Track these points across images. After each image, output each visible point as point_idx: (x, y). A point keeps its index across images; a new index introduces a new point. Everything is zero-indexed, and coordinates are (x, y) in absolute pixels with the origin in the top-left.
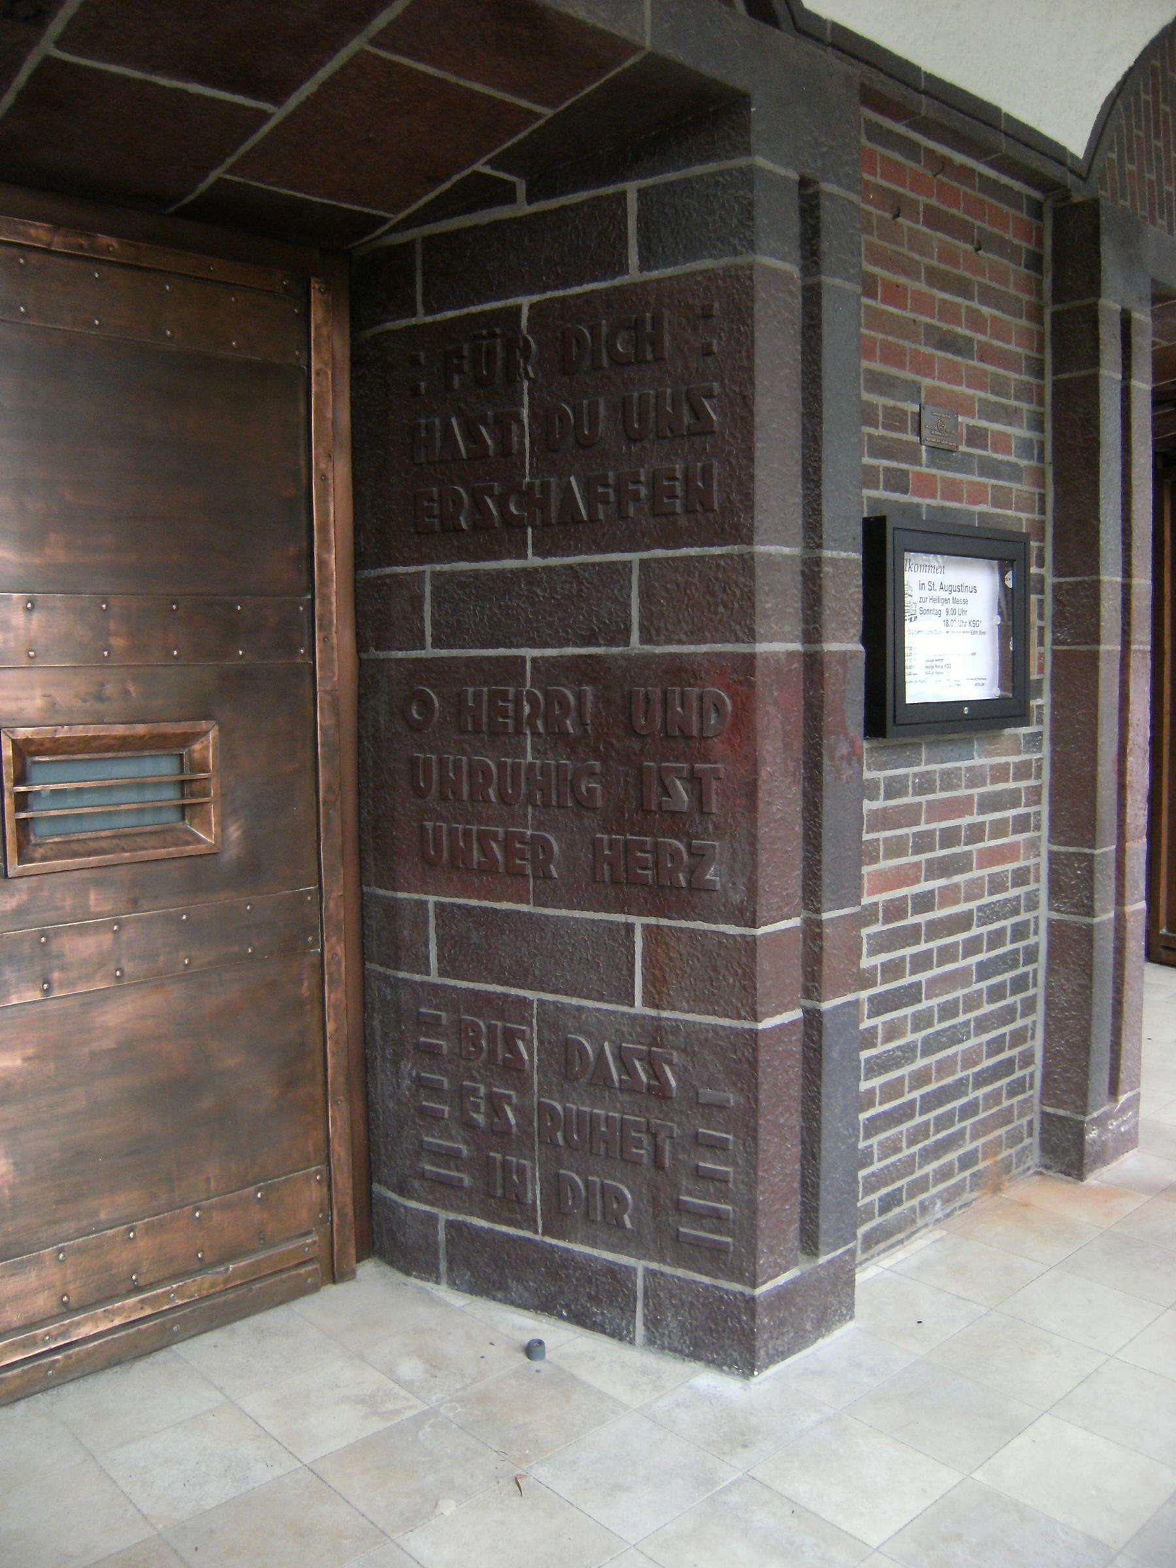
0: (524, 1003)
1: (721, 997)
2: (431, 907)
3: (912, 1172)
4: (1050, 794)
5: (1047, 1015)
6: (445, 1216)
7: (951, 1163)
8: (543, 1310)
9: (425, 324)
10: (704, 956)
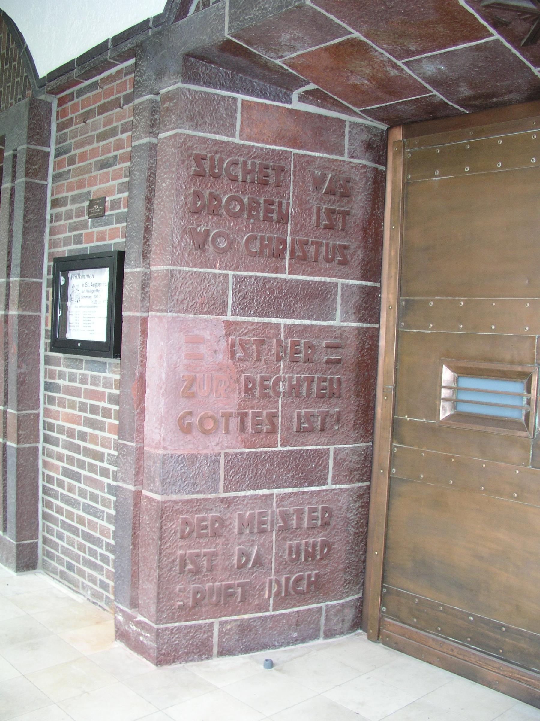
2: (237, 134)
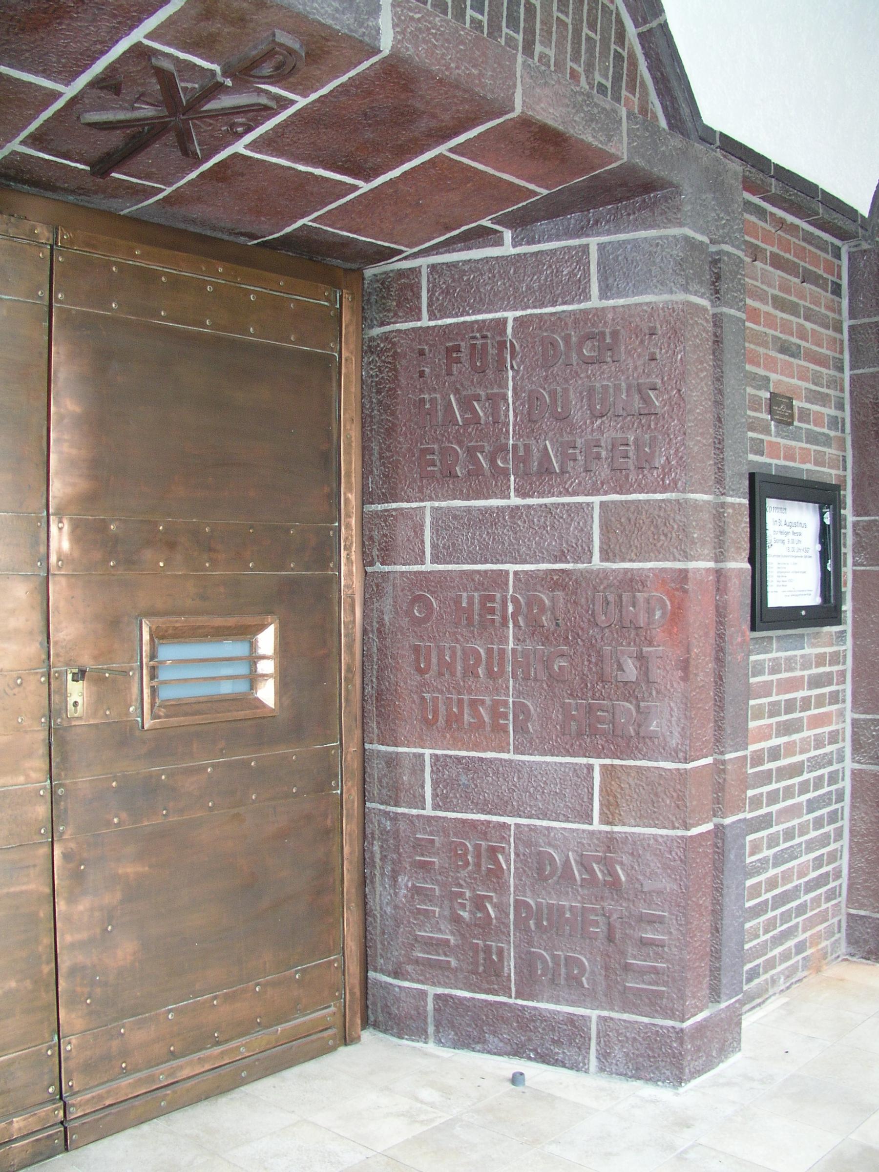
0: (505, 826)
1: (660, 814)
2: (427, 758)
3: (766, 954)
4: (852, 676)
5: (851, 840)
6: (432, 991)
7: (790, 949)
8: (514, 1055)
9: (428, 327)
10: (647, 785)
